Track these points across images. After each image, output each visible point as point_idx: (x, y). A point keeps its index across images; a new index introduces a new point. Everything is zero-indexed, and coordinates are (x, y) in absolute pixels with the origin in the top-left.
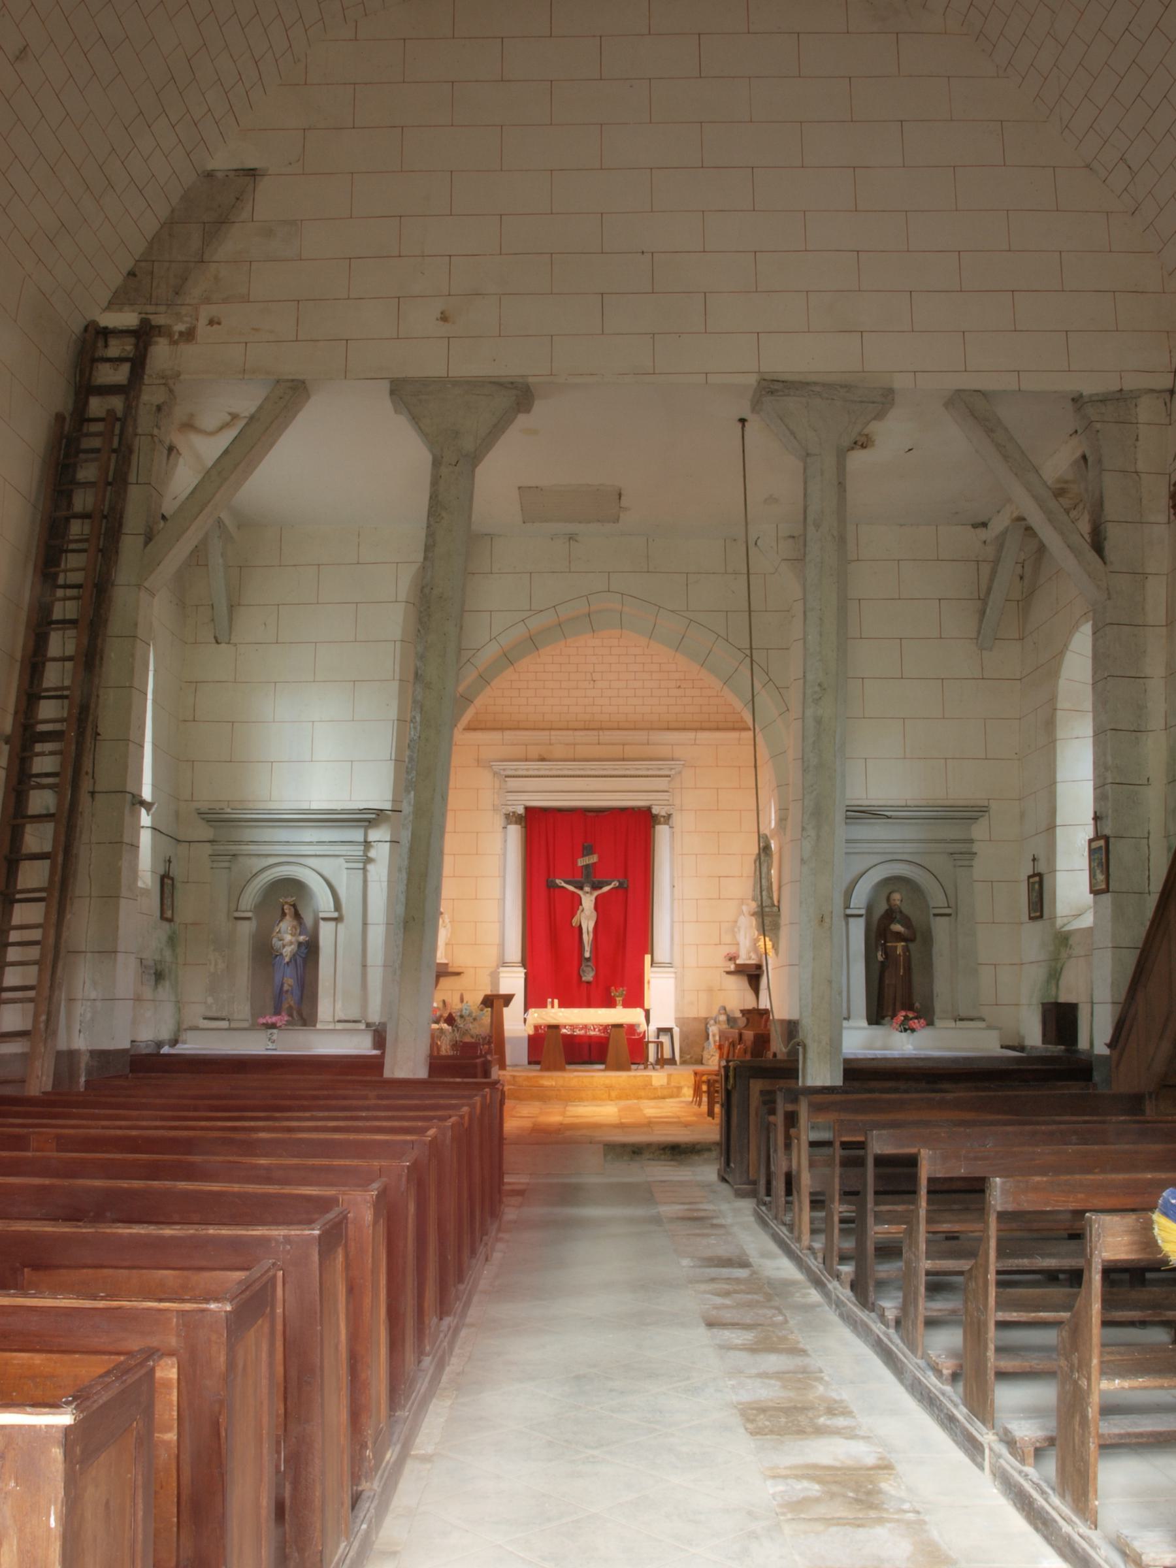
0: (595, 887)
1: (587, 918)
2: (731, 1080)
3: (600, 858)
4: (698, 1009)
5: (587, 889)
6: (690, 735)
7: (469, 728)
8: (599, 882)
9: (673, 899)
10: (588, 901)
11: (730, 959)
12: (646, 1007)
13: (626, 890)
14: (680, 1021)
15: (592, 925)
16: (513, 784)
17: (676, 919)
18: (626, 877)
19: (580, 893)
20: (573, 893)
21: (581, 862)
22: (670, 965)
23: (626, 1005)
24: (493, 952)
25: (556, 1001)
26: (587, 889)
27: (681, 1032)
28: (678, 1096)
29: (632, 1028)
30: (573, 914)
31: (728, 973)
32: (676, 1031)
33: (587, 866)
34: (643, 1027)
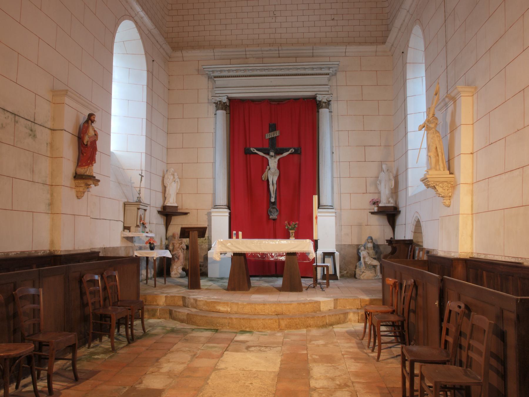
0: (278, 153)
1: (272, 174)
4: (352, 240)
5: (272, 153)
6: (342, 49)
10: (273, 163)
11: (374, 203)
12: (315, 238)
14: (339, 247)
15: (276, 179)
17: (335, 175)
19: (267, 157)
22: (332, 207)
23: (298, 237)
25: (240, 233)
26: (272, 153)
27: (340, 254)
28: (344, 322)
29: (304, 255)
30: (263, 172)
31: (372, 213)
32: (337, 254)
34: (312, 256)
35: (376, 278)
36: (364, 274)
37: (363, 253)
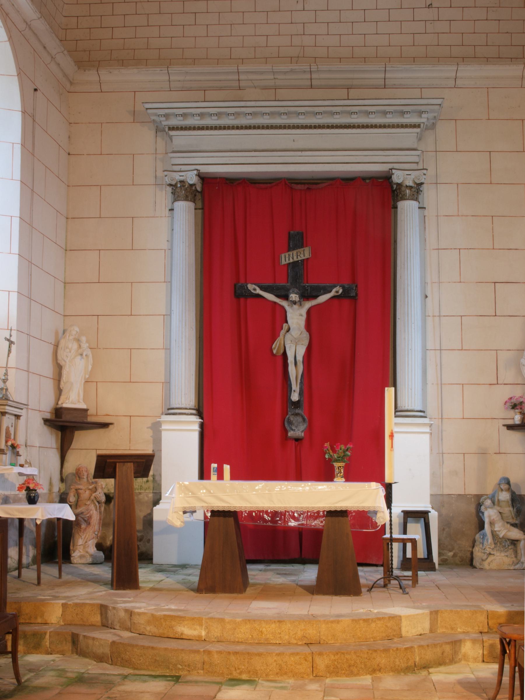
0: (306, 296)
1: (294, 341)
3: (314, 252)
5: (294, 297)
8: (313, 288)
9: (424, 316)
10: (296, 316)
11: (514, 407)
12: (387, 480)
13: (354, 299)
14: (438, 500)
15: (301, 351)
16: (181, 139)
17: (430, 346)
19: (284, 303)
20: (275, 303)
22: (422, 413)
23: (351, 476)
24: (156, 392)
25: (227, 468)
26: (294, 297)
27: (440, 516)
29: (363, 517)
30: (274, 336)
31: (510, 427)
32: (434, 516)
33: (295, 264)
34: (382, 517)
35: (517, 567)
36: (491, 558)
37: (490, 514)
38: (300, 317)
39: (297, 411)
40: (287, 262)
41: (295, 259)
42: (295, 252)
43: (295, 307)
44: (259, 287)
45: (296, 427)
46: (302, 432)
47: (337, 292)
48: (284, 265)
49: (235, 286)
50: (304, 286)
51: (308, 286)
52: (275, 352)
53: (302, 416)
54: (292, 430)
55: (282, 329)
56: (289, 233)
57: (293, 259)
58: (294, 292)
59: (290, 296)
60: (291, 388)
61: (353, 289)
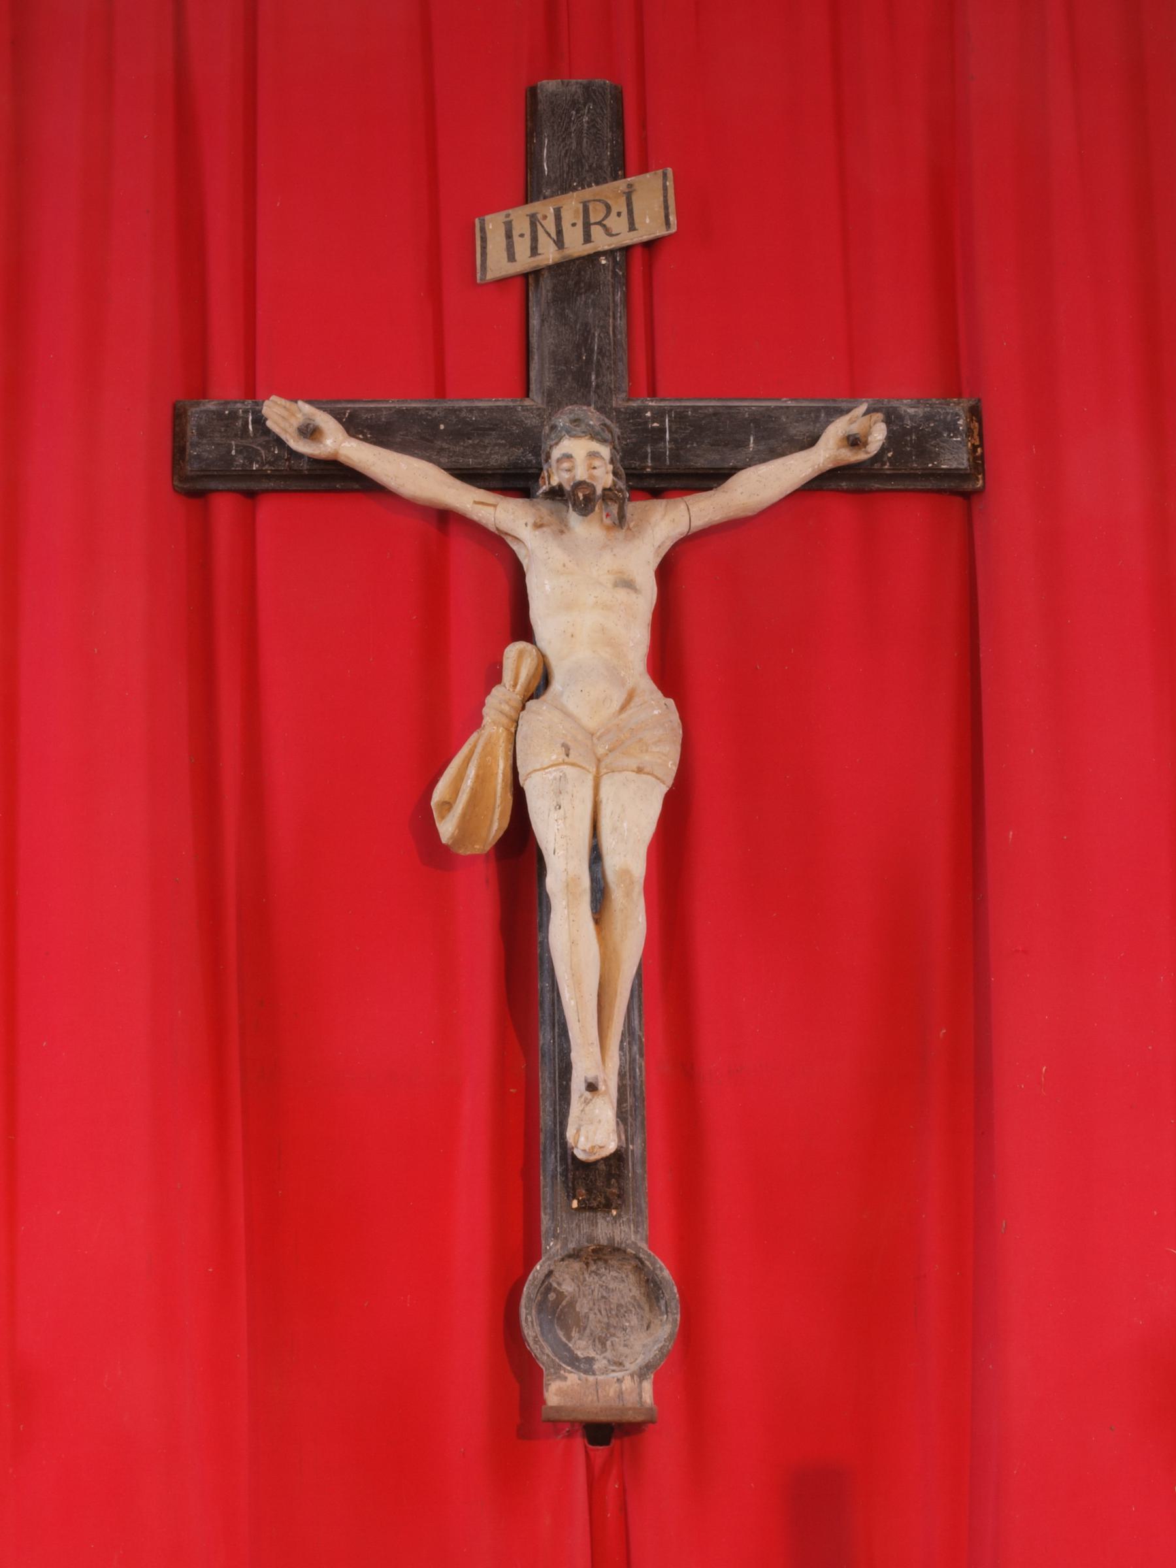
0: (651, 476)
1: (582, 748)
2: (630, 1100)
3: (690, 201)
7: (443, 818)
8: (693, 427)
10: (590, 592)
13: (961, 493)
18: (952, 371)
20: (445, 518)
21: (511, 243)
33: (573, 275)
38: (622, 594)
39: (605, 1229)
40: (524, 261)
41: (575, 246)
42: (571, 204)
43: (585, 529)
44: (337, 416)
45: (601, 1342)
46: (641, 1375)
47: (854, 442)
48: (502, 282)
49: (178, 416)
50: (639, 412)
51: (659, 414)
52: (447, 829)
53: (639, 1266)
54: (574, 1361)
55: (495, 677)
56: (533, 92)
57: (559, 242)
58: (578, 428)
59: (556, 453)
60: (565, 1070)
61: (952, 428)
